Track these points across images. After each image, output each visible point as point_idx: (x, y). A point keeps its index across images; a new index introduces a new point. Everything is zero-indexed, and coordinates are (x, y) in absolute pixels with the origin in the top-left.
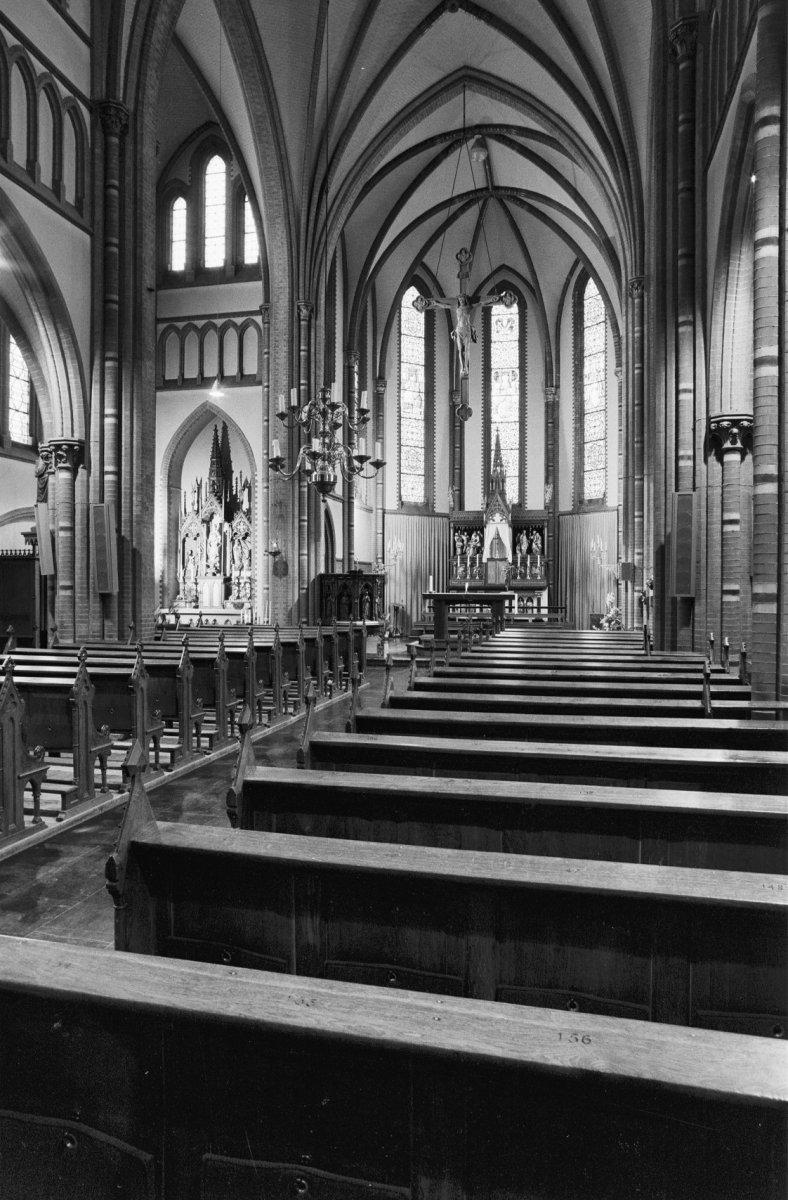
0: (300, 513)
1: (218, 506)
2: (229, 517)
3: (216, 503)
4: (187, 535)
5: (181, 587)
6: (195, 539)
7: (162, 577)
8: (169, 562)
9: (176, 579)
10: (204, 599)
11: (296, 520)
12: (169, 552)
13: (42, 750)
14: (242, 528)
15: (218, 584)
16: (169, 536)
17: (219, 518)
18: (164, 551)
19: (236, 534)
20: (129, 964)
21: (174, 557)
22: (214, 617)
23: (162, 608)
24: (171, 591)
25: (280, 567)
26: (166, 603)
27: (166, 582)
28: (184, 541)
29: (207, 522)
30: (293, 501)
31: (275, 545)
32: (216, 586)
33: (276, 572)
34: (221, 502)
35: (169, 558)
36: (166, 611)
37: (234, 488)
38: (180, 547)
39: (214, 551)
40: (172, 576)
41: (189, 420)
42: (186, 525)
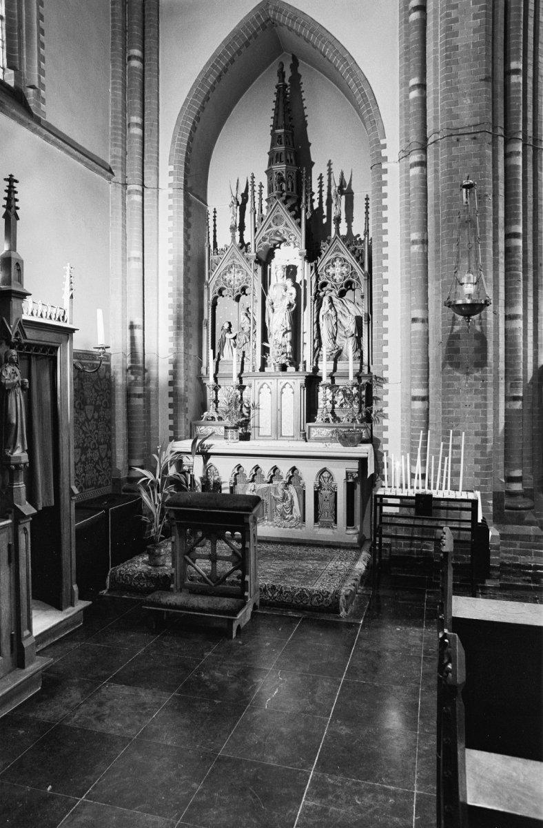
0: (510, 219)
1: (292, 223)
2: (312, 254)
3: (287, 217)
4: (220, 291)
5: (210, 394)
6: (237, 299)
7: (174, 373)
8: (187, 346)
9: (200, 379)
10: (263, 420)
11: (501, 234)
12: (187, 324)
13: (137, 124)
14: (338, 271)
15: (292, 389)
16: (187, 293)
17: (290, 254)
18: (178, 322)
19: (324, 284)
20: (43, 428)
21: (195, 335)
22: (293, 463)
23: (175, 438)
24: (191, 403)
25: (467, 348)
26: (183, 428)
27: (181, 384)
28: (214, 305)
29: (264, 260)
30: (495, 187)
31: (469, 289)
32: (287, 391)
33: (452, 355)
34: (299, 225)
35: (187, 336)
36: (186, 445)
37: (316, 197)
38: (207, 315)
39: (279, 321)
40: (192, 374)
41: (228, 43)
42: (219, 270)
